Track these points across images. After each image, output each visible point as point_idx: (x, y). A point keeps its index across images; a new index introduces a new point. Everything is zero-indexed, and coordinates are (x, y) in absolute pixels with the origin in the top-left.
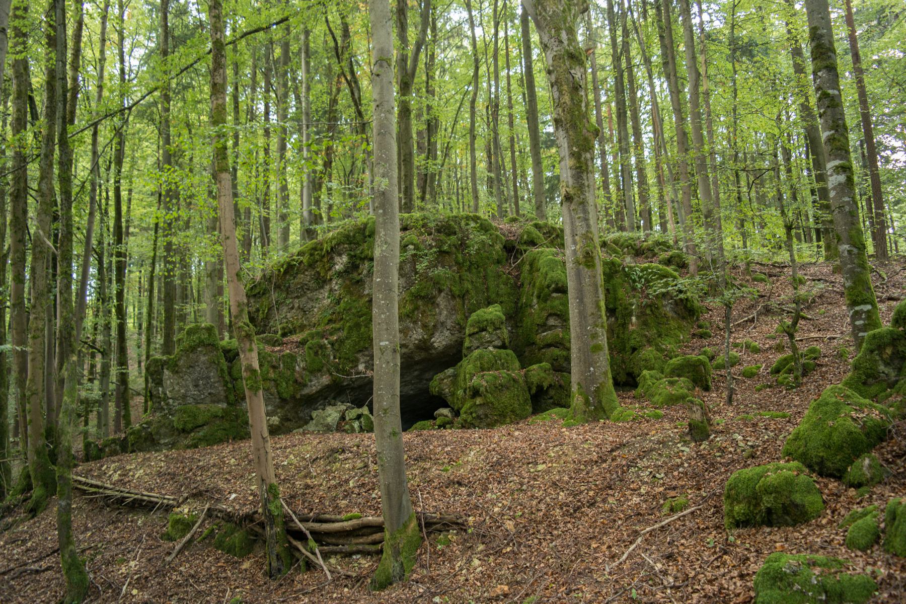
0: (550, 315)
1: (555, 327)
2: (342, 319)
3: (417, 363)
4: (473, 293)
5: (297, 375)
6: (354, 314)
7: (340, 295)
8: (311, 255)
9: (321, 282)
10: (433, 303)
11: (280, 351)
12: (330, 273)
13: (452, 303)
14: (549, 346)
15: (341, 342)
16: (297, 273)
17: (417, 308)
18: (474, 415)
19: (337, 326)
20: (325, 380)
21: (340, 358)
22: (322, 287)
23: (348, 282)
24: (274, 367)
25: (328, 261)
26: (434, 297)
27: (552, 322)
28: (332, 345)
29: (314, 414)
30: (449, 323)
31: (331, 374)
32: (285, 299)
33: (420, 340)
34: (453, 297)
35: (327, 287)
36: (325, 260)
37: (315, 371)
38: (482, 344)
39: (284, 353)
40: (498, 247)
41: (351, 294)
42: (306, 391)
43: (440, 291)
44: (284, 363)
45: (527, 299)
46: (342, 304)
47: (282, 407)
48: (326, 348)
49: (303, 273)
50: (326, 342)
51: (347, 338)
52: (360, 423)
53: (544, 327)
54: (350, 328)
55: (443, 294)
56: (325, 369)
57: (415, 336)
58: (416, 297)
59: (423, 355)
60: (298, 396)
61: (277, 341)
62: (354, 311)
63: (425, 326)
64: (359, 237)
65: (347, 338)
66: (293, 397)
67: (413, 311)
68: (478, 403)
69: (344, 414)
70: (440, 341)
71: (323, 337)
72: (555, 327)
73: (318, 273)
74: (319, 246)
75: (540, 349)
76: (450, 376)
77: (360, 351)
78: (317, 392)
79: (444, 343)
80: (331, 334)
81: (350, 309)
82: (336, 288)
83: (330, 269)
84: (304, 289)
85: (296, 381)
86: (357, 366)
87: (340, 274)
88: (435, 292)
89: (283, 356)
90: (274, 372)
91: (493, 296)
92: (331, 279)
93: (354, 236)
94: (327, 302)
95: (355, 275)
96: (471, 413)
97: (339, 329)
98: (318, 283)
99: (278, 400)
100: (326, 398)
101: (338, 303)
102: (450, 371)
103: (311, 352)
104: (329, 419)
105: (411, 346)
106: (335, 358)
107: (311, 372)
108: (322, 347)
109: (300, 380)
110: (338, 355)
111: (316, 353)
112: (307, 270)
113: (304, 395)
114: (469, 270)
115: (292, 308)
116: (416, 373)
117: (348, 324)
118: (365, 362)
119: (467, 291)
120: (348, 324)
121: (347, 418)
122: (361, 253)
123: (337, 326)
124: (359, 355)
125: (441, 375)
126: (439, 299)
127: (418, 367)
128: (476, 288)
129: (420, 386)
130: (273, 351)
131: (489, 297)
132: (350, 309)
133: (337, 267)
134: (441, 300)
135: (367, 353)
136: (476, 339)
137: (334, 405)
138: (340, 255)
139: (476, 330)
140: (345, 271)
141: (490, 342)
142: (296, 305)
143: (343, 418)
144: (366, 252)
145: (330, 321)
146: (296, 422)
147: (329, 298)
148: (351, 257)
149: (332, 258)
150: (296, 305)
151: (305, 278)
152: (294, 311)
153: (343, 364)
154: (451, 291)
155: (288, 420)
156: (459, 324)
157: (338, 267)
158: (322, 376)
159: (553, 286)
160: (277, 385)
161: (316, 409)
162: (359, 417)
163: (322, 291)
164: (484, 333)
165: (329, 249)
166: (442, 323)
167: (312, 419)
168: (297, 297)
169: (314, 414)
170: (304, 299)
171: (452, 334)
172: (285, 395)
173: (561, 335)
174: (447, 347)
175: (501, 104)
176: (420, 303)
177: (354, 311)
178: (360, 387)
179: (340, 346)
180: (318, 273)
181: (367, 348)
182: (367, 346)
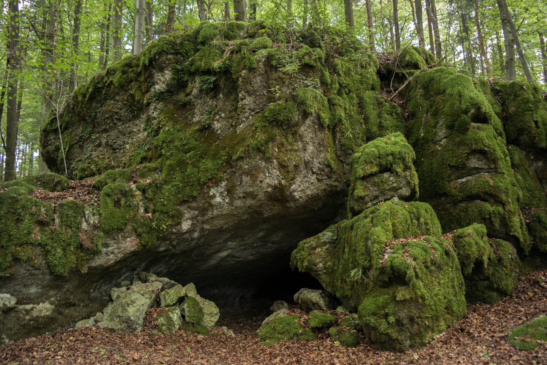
0: (474, 152)
1: (478, 170)
2: (160, 155)
3: (266, 220)
4: (346, 123)
5: (82, 236)
6: (176, 147)
7: (159, 123)
8: (124, 72)
9: (137, 109)
10: (294, 134)
11: (58, 198)
12: (148, 96)
13: (320, 135)
14: (471, 198)
15: (157, 187)
16: (106, 99)
17: (272, 139)
18: (392, 319)
19: (152, 165)
20: (130, 244)
21: (154, 212)
22: (136, 117)
23: (171, 107)
24: (42, 224)
25: (146, 80)
26: (297, 125)
27: (474, 162)
28: (144, 191)
29: (115, 293)
30: (316, 165)
31: (139, 235)
32: (90, 134)
33: (275, 187)
34: (321, 126)
35: (144, 116)
36: (142, 79)
37: (112, 232)
38: (383, 193)
39: (64, 201)
40: (372, 70)
41: (176, 122)
42: (98, 261)
43: (305, 115)
44: (61, 217)
45: (427, 132)
46: (161, 136)
47: (58, 288)
48: (133, 196)
49: (113, 98)
50: (133, 186)
51: (166, 182)
52: (183, 310)
53: (461, 169)
54: (171, 168)
55: (308, 122)
56: (129, 228)
57: (267, 180)
58: (270, 123)
59: (277, 209)
60: (85, 270)
61: (59, 183)
62: (177, 143)
63: (282, 166)
64: (189, 46)
65: (166, 182)
66: (76, 272)
67: (267, 142)
68: (399, 297)
69: (158, 296)
70: (304, 187)
71: (130, 179)
72: (478, 170)
73: (132, 96)
74: (135, 62)
75: (456, 203)
76: (325, 243)
77: (185, 202)
78: (117, 263)
79: (309, 192)
80: (143, 176)
81: (172, 141)
82: (155, 115)
83: (147, 91)
84: (115, 119)
85: (81, 247)
86: (179, 224)
87: (160, 97)
88: (296, 117)
89: (61, 205)
90: (42, 231)
91: (375, 129)
92: (148, 104)
93: (181, 44)
94: (143, 135)
95: (181, 97)
96: (386, 316)
97: (155, 169)
98: (132, 111)
99: (48, 277)
100: (134, 269)
101: (157, 132)
102: (327, 235)
103: (108, 200)
104: (131, 311)
105: (261, 196)
106: (146, 211)
107: (107, 233)
108: (126, 194)
109: (87, 244)
110: (152, 206)
111: (117, 203)
112: (117, 94)
113: (96, 268)
114: (339, 93)
115: (99, 145)
116: (261, 234)
117: (168, 162)
118: (192, 219)
119: (340, 121)
120: (168, 162)
121: (163, 304)
122: (191, 65)
123: (152, 165)
124: (183, 208)
125: (311, 241)
126: (302, 129)
127: (265, 226)
128: (351, 116)
129: (263, 250)
130: (45, 198)
131: (368, 131)
132: (172, 141)
133: (157, 87)
134: (306, 130)
135: (194, 204)
136: (374, 184)
137: (145, 281)
138: (161, 70)
139: (375, 169)
140: (168, 91)
141: (395, 190)
142: (104, 141)
143: (157, 302)
144: (198, 63)
145: (144, 159)
146: (86, 306)
147: (145, 130)
148: (176, 72)
149: (151, 76)
150: (104, 141)
151: (115, 105)
152: (101, 149)
153: (159, 220)
154: (319, 117)
155: (70, 305)
156: (329, 166)
157: (159, 87)
158: (125, 238)
159: (473, 111)
160: (46, 253)
161: (118, 286)
162: (181, 300)
163: (137, 122)
164: (386, 175)
165: (147, 62)
166: (307, 163)
167: (112, 300)
168: (105, 131)
169: (115, 293)
170: (113, 133)
171: (319, 180)
172: (60, 270)
173: (491, 182)
174: (313, 199)
175: (148, 302)
176: (276, 131)
177: (177, 143)
178: (184, 252)
179: (155, 193)
180: (132, 96)
181: (194, 198)
182: (195, 194)
